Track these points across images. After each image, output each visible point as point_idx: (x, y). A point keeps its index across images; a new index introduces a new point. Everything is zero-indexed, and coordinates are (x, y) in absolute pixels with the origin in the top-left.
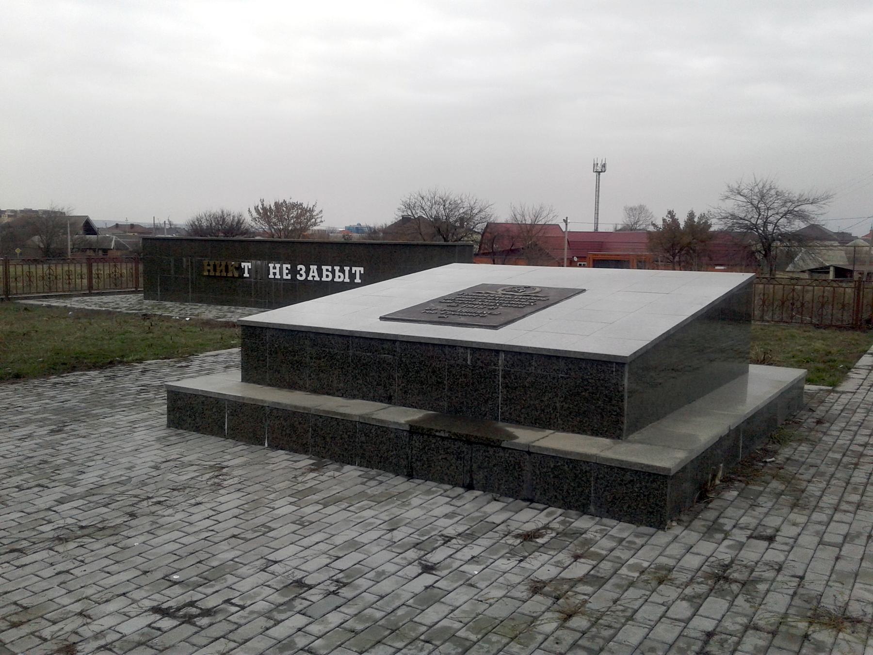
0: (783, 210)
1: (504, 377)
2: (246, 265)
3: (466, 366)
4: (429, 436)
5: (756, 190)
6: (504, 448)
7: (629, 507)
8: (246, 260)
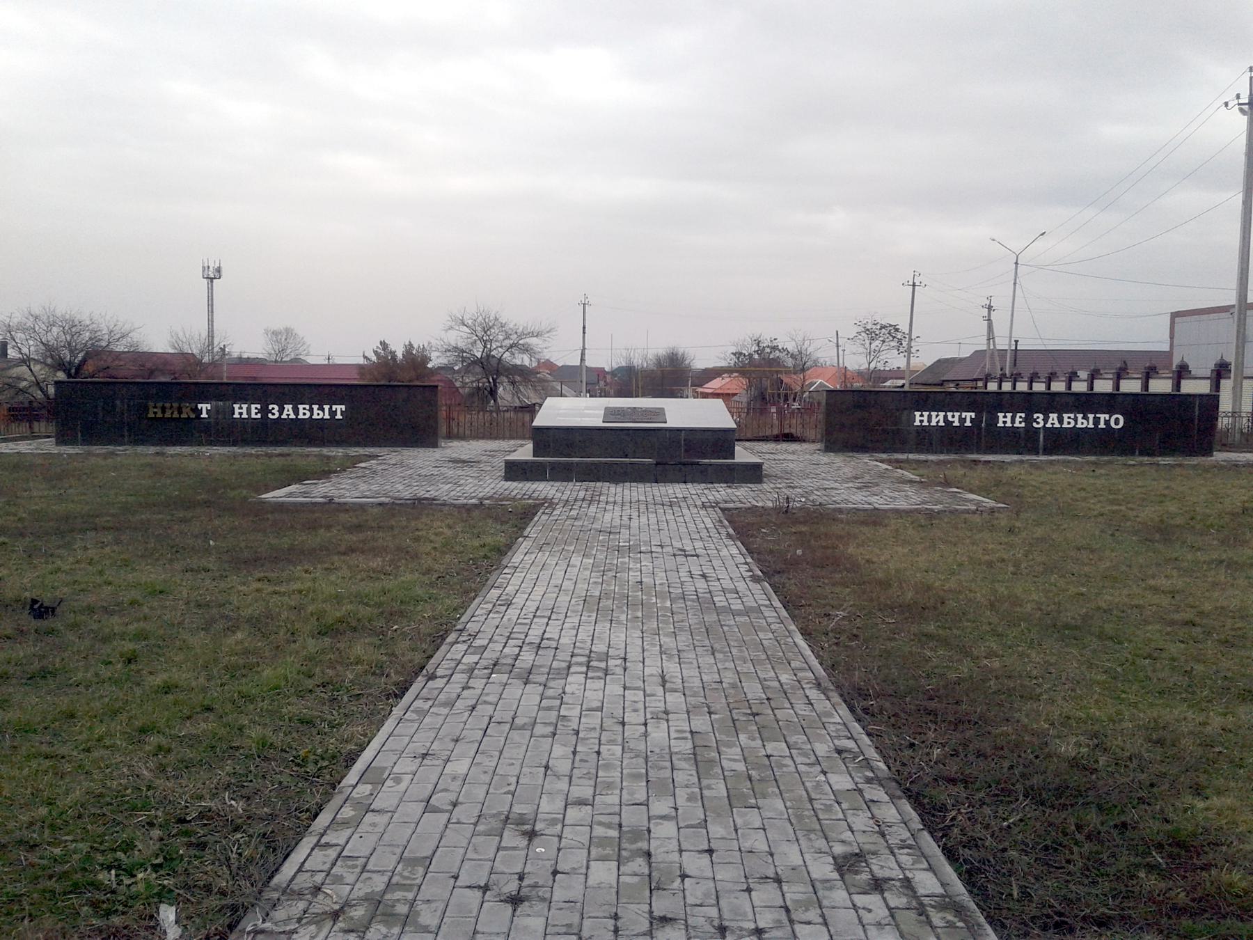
0: (508, 343)
2: (204, 407)
8: (205, 400)
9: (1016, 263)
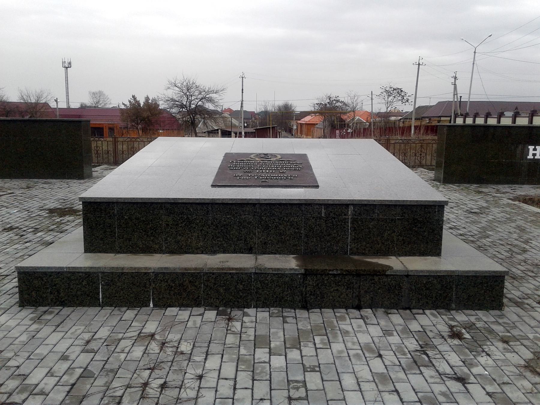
1: (352, 223)
3: (321, 218)
4: (322, 275)
5: (185, 84)
6: (387, 276)
7: (479, 300)
9: (475, 52)
